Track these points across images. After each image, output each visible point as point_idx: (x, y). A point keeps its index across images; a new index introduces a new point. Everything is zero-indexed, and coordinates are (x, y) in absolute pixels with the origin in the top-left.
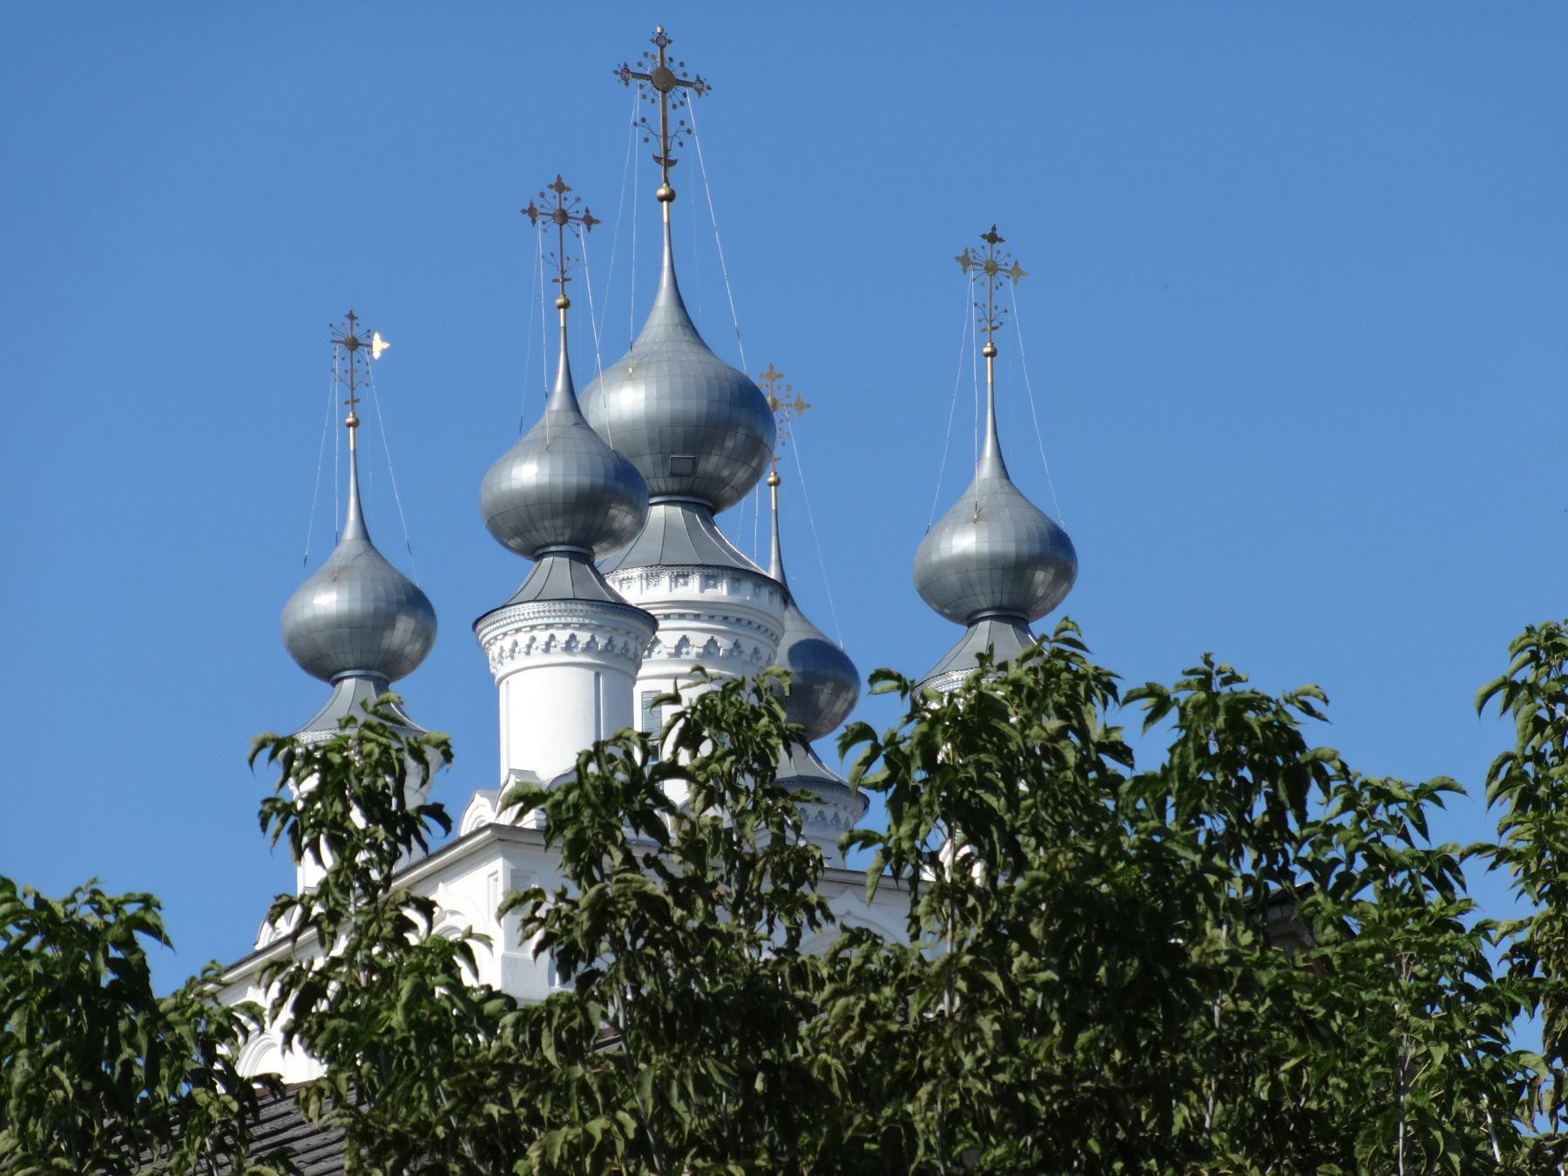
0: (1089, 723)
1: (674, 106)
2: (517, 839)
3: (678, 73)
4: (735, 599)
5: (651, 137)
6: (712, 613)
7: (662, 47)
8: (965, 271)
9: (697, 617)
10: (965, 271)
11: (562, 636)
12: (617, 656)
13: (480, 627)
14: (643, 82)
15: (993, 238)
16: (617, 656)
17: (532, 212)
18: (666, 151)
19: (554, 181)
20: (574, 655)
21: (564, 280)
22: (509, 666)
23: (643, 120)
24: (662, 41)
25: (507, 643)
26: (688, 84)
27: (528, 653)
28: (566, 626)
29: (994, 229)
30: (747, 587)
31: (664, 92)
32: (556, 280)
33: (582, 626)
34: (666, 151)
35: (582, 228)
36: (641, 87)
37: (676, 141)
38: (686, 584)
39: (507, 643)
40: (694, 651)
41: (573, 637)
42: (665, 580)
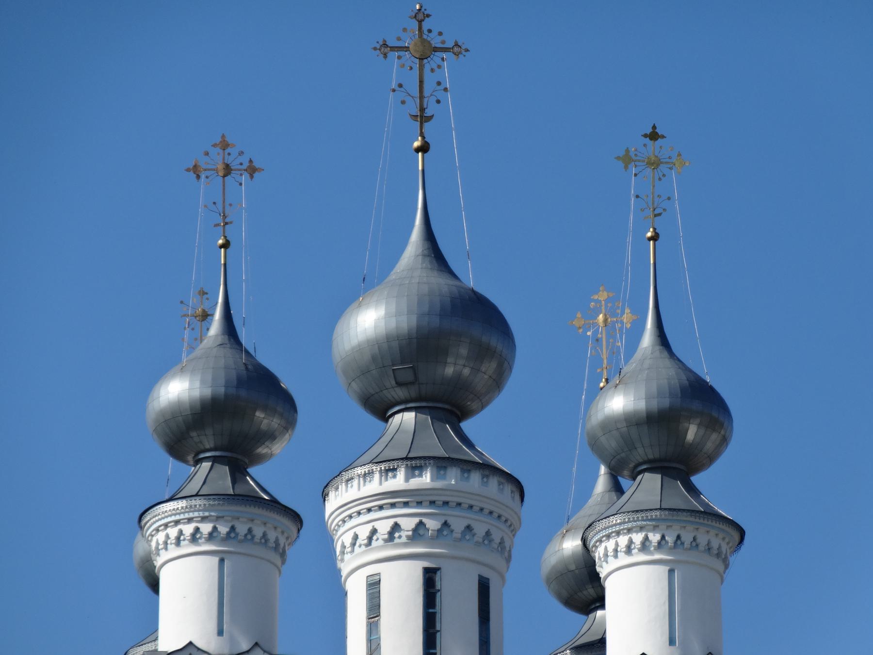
0: (332, 495)
1: (432, 70)
3: (436, 42)
4: (439, 484)
5: (408, 99)
6: (419, 499)
7: (420, 22)
8: (626, 168)
9: (406, 504)
10: (626, 168)
12: (241, 542)
13: (143, 523)
14: (401, 53)
16: (477, 544)
17: (196, 170)
18: (422, 110)
19: (218, 140)
20: (199, 545)
21: (226, 223)
22: (613, 564)
23: (400, 86)
24: (420, 17)
25: (610, 544)
27: (166, 549)
28: (190, 520)
29: (654, 127)
30: (476, 477)
31: (421, 59)
32: (217, 225)
33: (204, 519)
34: (422, 110)
35: (245, 178)
36: (399, 57)
37: (433, 99)
38: (394, 477)
39: (161, 537)
40: (404, 534)
41: (197, 530)
42: (401, 474)
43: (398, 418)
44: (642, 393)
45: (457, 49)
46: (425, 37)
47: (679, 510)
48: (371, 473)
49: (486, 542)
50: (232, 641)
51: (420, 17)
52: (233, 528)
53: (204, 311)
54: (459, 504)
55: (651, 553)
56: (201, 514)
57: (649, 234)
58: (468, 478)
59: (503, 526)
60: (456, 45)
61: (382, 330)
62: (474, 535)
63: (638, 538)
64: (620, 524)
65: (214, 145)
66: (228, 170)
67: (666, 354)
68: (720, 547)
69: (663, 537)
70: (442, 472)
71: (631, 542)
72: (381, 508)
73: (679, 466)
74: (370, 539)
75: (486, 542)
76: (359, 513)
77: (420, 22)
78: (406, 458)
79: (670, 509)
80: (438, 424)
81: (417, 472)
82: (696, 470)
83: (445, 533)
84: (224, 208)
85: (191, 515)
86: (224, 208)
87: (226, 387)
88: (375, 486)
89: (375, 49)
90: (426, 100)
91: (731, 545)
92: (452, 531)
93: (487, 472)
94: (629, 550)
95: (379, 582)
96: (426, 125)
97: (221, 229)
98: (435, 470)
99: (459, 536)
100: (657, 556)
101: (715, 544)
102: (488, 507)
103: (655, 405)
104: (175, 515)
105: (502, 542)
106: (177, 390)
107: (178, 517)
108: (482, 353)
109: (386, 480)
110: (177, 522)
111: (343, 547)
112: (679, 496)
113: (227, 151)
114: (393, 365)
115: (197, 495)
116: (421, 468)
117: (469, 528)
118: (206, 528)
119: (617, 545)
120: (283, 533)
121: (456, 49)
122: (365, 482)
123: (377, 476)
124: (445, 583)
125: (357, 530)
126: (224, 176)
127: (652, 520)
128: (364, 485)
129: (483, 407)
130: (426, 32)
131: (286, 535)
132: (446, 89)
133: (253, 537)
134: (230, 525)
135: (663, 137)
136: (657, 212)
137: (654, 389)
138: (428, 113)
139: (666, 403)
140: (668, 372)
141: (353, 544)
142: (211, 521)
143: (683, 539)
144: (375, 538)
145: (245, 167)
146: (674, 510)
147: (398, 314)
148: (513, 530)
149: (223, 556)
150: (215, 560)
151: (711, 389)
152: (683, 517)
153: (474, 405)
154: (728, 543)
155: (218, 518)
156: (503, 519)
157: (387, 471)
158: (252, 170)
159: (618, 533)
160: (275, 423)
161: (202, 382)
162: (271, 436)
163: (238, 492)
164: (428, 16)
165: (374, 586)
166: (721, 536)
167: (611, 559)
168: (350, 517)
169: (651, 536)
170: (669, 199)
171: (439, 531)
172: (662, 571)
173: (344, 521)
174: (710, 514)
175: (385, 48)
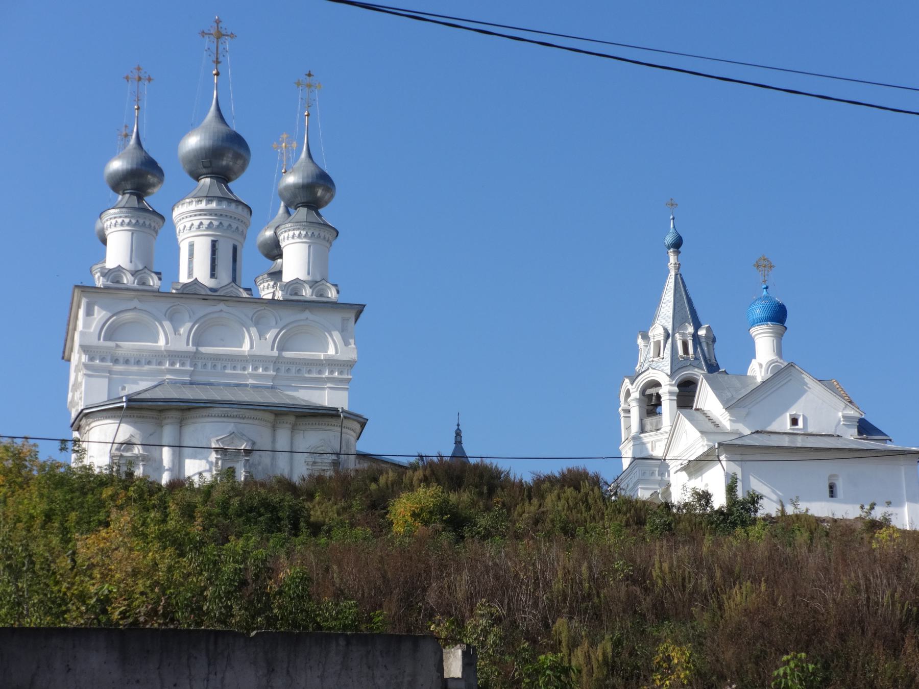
0: (176, 209)
3: (224, 32)
4: (219, 207)
11: (297, 233)
15: (309, 75)
17: (127, 78)
22: (287, 242)
25: (286, 235)
30: (233, 206)
33: (126, 217)
35: (146, 83)
42: (204, 203)
45: (232, 36)
50: (136, 265)
61: (198, 146)
63: (297, 233)
66: (140, 79)
82: (321, 207)
88: (194, 207)
94: (293, 237)
100: (304, 240)
101: (327, 236)
103: (306, 181)
106: (117, 165)
108: (237, 156)
117: (230, 225)
118: (127, 220)
124: (219, 246)
139: (310, 180)
140: (311, 169)
148: (247, 225)
153: (233, 177)
162: (153, 185)
165: (191, 246)
175: (203, 33)
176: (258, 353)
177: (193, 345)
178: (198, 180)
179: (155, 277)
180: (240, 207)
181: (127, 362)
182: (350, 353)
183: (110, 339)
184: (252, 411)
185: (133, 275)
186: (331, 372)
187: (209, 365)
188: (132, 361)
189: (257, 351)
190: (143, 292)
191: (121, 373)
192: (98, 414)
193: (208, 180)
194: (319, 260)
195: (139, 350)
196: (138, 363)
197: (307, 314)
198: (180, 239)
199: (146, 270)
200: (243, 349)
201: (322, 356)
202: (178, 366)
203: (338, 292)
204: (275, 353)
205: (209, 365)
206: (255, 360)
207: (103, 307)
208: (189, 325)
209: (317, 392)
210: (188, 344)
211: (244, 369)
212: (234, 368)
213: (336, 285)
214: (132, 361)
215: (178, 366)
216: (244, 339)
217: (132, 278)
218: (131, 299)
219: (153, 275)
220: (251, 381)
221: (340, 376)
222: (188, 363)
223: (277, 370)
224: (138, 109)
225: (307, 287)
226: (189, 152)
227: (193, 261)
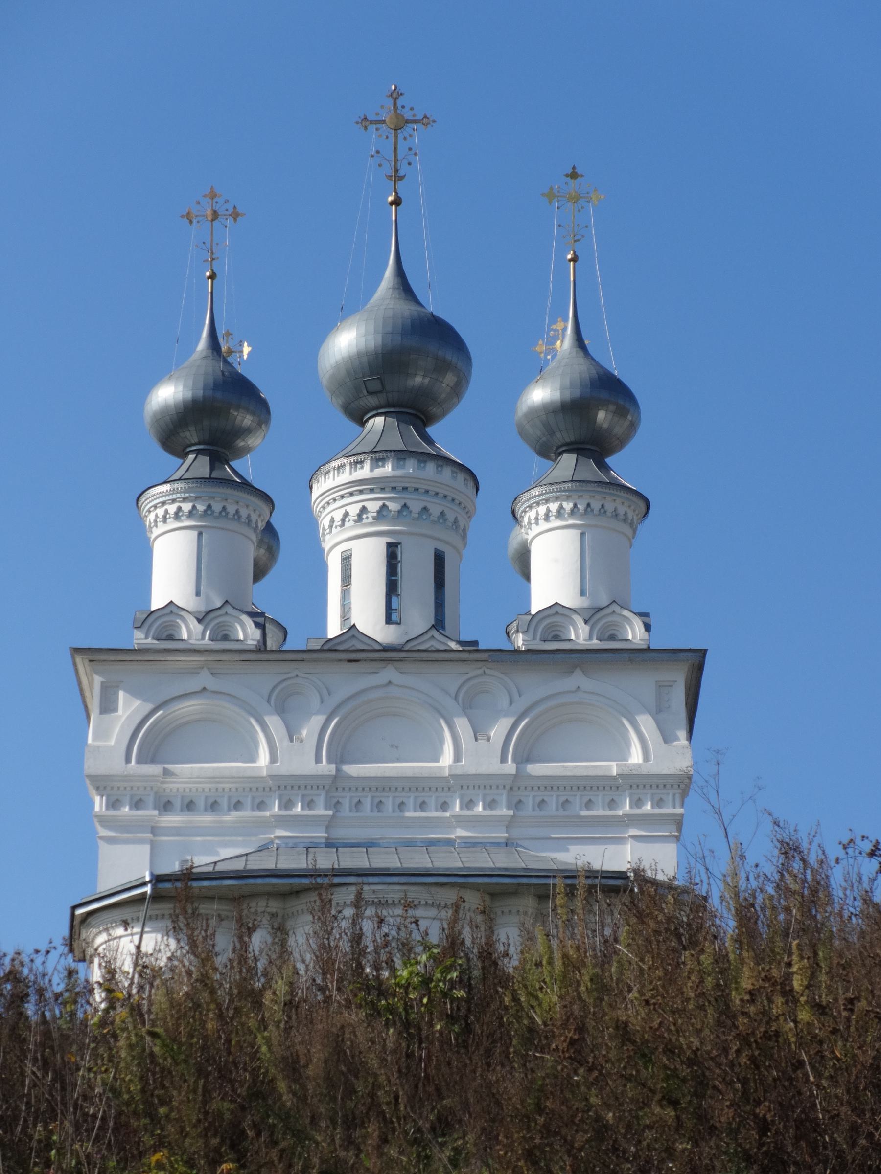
0: (315, 486)
1: (405, 139)
2: (167, 658)
3: (408, 115)
4: (399, 473)
7: (395, 100)
8: (550, 203)
9: (372, 491)
10: (550, 203)
11: (554, 507)
12: (216, 517)
13: (140, 504)
14: (379, 126)
16: (433, 522)
18: (396, 170)
21: (213, 259)
25: (532, 514)
26: (416, 122)
27: (156, 526)
28: (174, 501)
29: (574, 168)
30: (431, 467)
33: (185, 500)
34: (396, 170)
35: (229, 222)
36: (377, 129)
37: (406, 162)
38: (362, 468)
41: (179, 509)
42: (367, 465)
43: (371, 421)
44: (557, 385)
45: (425, 121)
46: (399, 111)
47: (588, 482)
48: (342, 466)
49: (441, 521)
50: (208, 600)
51: (395, 96)
52: (209, 507)
53: (229, 348)
54: (416, 489)
55: (566, 520)
56: (183, 495)
57: (569, 257)
58: (424, 467)
59: (456, 508)
60: (425, 117)
61: (354, 350)
62: (430, 515)
63: (554, 507)
64: (539, 495)
65: (204, 196)
66: (215, 215)
67: (582, 354)
68: (625, 514)
69: (575, 506)
70: (402, 463)
71: (548, 510)
72: (351, 494)
73: (594, 447)
74: (343, 521)
75: (441, 521)
76: (335, 500)
77: (395, 100)
78: (371, 452)
79: (580, 481)
80: (403, 425)
81: (380, 464)
82: (610, 452)
83: (405, 513)
84: (212, 246)
85: (175, 496)
86: (212, 246)
87: (204, 389)
88: (346, 476)
89: (357, 123)
90: (399, 164)
91: (637, 512)
92: (411, 512)
93: (440, 463)
94: (547, 517)
95: (350, 557)
96: (399, 183)
97: (209, 263)
98: (395, 461)
99: (417, 515)
100: (571, 522)
101: (621, 510)
102: (442, 492)
103: (568, 396)
104: (162, 497)
105: (456, 522)
106: (168, 394)
107: (164, 499)
108: (442, 367)
109: (356, 470)
110: (163, 503)
111: (324, 529)
112: (590, 469)
113: (215, 200)
114: (364, 377)
115: (180, 479)
116: (383, 460)
117: (425, 509)
118: (187, 507)
119: (537, 514)
120: (255, 511)
121: (425, 121)
122: (339, 473)
123: (348, 467)
124: (405, 557)
125: (333, 514)
126: (212, 221)
127: (564, 491)
128: (338, 476)
129: (444, 414)
130: (400, 107)
131: (257, 512)
132: (415, 154)
133: (227, 514)
134: (207, 504)
135: (582, 176)
136: (576, 238)
137: (567, 382)
138: (401, 173)
139: (577, 393)
140: (581, 368)
141: (331, 527)
142: (191, 501)
143: (592, 506)
144: (347, 519)
145: (230, 212)
146: (584, 481)
147: (366, 334)
148: (469, 515)
149: (201, 529)
150: (195, 533)
151: (619, 382)
152: (591, 487)
153: (434, 410)
154: (634, 511)
155: (196, 498)
156: (463, 506)
157: (357, 463)
158: (235, 215)
159: (538, 504)
160: (247, 420)
161: (185, 386)
162: (247, 432)
163: (213, 476)
164: (402, 95)
165: (346, 560)
166: (627, 504)
167: (533, 526)
168: (328, 503)
169: (565, 504)
170: (587, 227)
171: (399, 512)
172: (575, 534)
173: (324, 508)
174: (615, 484)
175: (365, 122)
176: (472, 771)
177: (329, 761)
178: (363, 423)
179: (249, 622)
180: (447, 471)
181: (189, 806)
182: (677, 757)
183: (153, 761)
184: (433, 889)
185: (200, 621)
186: (638, 803)
187: (367, 803)
188: (201, 803)
189: (469, 766)
190: (222, 654)
191: (177, 831)
192: (104, 915)
193: (380, 420)
194: (600, 565)
195: (213, 779)
196: (213, 806)
197: (578, 679)
198: (326, 546)
199: (229, 609)
200: (441, 763)
201: (613, 768)
202: (298, 809)
203: (648, 628)
204: (510, 767)
205: (367, 803)
206: (465, 785)
207: (135, 692)
208: (317, 721)
209: (611, 848)
210: (318, 760)
211: (444, 806)
212: (423, 806)
213: (641, 615)
214: (201, 803)
215: (298, 809)
216: (442, 742)
217: (200, 628)
218: (194, 671)
219: (245, 618)
220: (461, 833)
221: (657, 811)
222: (321, 800)
223: (518, 805)
224: (212, 277)
225: (579, 621)
226: (337, 366)
227: (354, 598)
